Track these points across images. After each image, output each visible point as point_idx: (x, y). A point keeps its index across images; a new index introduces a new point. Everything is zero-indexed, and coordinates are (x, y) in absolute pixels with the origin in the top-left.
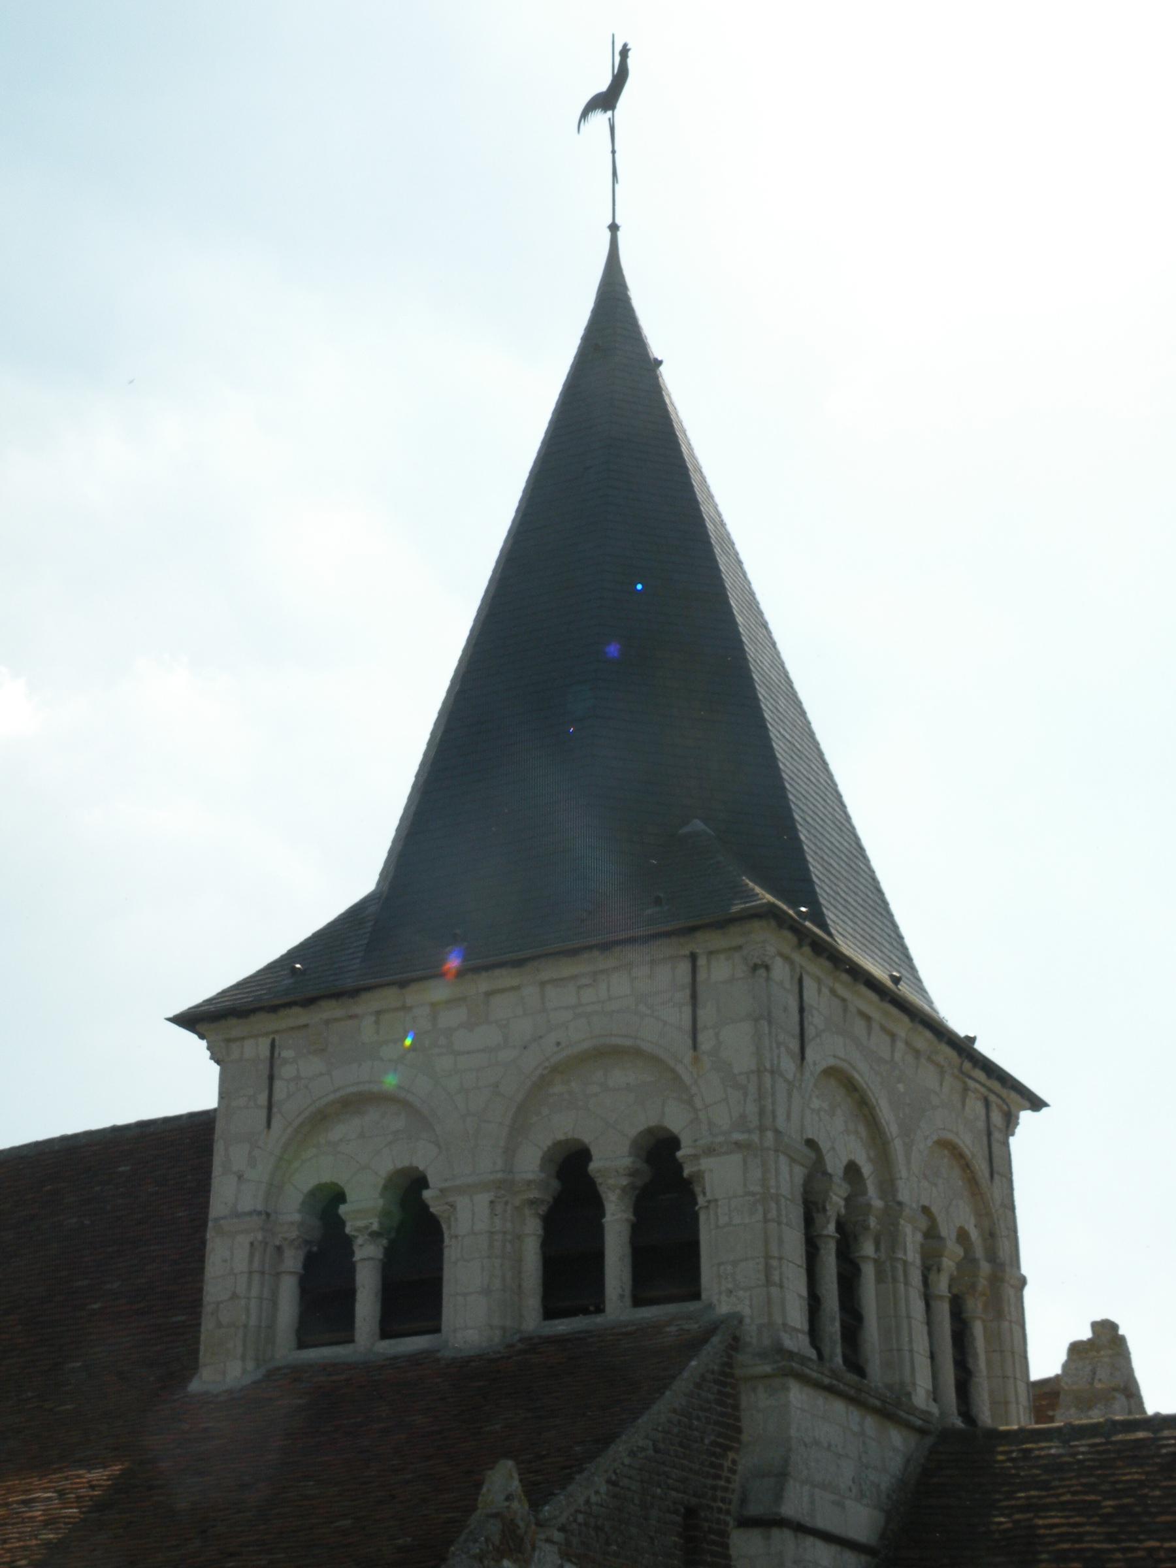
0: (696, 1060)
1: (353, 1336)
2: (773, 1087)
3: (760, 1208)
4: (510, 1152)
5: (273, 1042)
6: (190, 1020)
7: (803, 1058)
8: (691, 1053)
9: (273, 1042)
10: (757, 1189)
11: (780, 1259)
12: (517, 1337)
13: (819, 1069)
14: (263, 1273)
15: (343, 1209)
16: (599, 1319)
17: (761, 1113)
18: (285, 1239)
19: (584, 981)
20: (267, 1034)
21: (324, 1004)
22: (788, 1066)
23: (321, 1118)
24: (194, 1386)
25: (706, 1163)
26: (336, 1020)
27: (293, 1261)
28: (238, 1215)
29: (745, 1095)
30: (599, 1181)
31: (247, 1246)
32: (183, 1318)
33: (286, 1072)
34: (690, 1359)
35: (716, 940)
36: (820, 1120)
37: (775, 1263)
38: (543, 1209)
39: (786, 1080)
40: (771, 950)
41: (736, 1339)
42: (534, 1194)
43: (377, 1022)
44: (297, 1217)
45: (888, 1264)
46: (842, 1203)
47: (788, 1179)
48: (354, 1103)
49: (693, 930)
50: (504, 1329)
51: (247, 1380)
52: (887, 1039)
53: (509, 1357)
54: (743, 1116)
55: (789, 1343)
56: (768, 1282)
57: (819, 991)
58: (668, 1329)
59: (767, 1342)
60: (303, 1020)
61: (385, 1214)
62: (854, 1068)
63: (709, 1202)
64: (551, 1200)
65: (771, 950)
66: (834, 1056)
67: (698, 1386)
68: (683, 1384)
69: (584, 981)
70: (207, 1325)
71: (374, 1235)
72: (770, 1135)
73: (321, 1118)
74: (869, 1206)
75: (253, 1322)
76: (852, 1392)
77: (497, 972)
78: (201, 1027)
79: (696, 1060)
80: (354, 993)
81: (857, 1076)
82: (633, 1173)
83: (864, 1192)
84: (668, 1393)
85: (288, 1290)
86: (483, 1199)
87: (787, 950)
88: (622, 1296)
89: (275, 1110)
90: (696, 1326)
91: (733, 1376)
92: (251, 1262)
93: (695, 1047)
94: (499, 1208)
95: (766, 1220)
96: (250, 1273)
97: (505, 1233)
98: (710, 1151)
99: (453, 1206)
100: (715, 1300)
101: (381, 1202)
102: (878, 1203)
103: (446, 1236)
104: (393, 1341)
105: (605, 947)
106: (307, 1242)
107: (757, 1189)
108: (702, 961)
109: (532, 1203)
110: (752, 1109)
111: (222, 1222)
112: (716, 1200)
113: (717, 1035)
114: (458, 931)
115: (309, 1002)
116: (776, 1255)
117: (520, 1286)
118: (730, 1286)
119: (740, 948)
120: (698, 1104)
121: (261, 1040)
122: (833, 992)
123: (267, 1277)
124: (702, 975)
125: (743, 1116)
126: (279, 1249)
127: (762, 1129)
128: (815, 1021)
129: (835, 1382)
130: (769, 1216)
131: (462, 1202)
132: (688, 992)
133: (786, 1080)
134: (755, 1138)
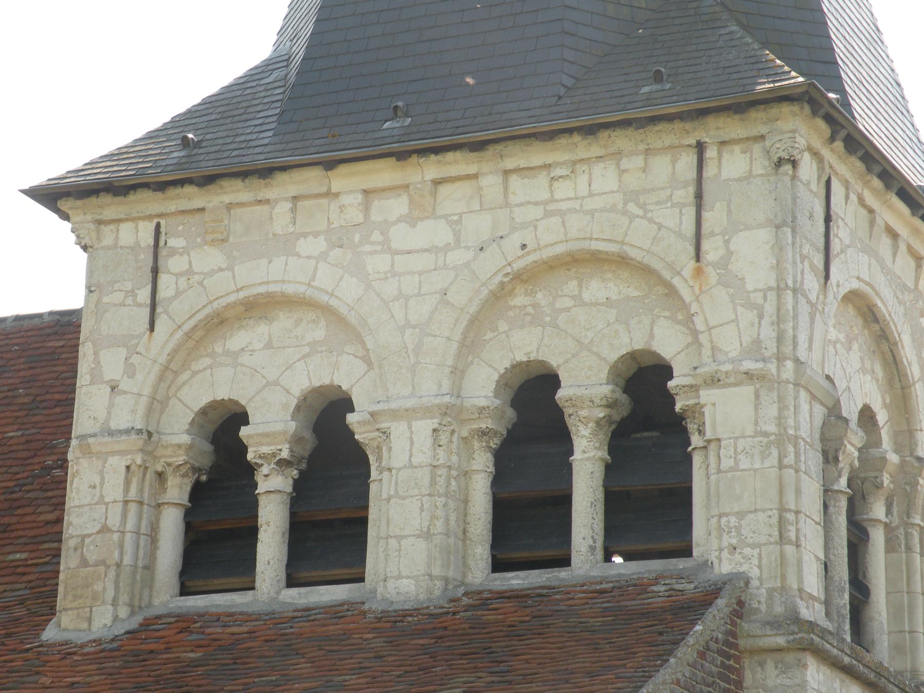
0: (699, 272)
1: (254, 582)
2: (795, 308)
3: (775, 453)
4: (458, 372)
5: (158, 226)
6: (51, 196)
7: (827, 277)
8: (692, 263)
9: (158, 226)
10: (772, 428)
11: (797, 512)
12: (461, 591)
13: (843, 291)
14: (141, 503)
15: (244, 432)
16: (562, 574)
17: (780, 339)
18: (169, 465)
19: (558, 172)
20: (149, 217)
21: (225, 183)
22: (812, 283)
23: (217, 323)
24: (50, 634)
25: (707, 396)
26: (241, 205)
27: (178, 491)
28: (111, 433)
29: (761, 317)
30: (567, 411)
31: (123, 470)
32: (24, 556)
33: (173, 264)
34: (694, 623)
35: (732, 127)
36: (837, 353)
37: (791, 517)
38: (495, 443)
39: (809, 302)
40: (801, 142)
41: (741, 603)
42: (487, 424)
43: (293, 210)
44: (185, 439)
45: (902, 530)
46: (856, 454)
47: (807, 419)
48: (257, 307)
49: (703, 113)
50: (446, 580)
51: (119, 630)
52: (912, 263)
53: (454, 613)
54: (757, 342)
55: (806, 613)
56: (782, 539)
57: (847, 197)
58: (655, 588)
59: (779, 609)
60: (198, 203)
61: (297, 440)
62: (877, 294)
63: (709, 441)
64: (505, 433)
65: (801, 142)
66: (858, 278)
67: (702, 655)
68: (687, 651)
69: (558, 172)
70: (68, 562)
71: (283, 464)
72: (789, 364)
73: (217, 323)
74: (884, 460)
75: (127, 560)
76: (872, 676)
77: (450, 156)
78: (63, 205)
79: (699, 272)
80: (266, 172)
81: (880, 304)
82: (611, 405)
83: (878, 443)
84: (672, 660)
85: (171, 525)
86: (424, 427)
87: (817, 144)
88: (592, 549)
89: (159, 310)
90: (692, 586)
91: (735, 646)
92: (127, 489)
93: (698, 258)
94: (444, 439)
95: (781, 466)
96: (126, 502)
97: (450, 467)
98: (714, 381)
99: (386, 433)
100: (713, 557)
101: (292, 426)
102: (893, 458)
103: (373, 469)
104: (302, 590)
105: (590, 131)
106: (195, 470)
107: (772, 428)
108: (711, 153)
109: (483, 433)
110: (768, 333)
111: (91, 440)
112: (719, 440)
113: (727, 242)
114: (400, 104)
115: (207, 180)
116: (793, 507)
117: (465, 532)
118: (734, 541)
119: (762, 137)
120: (699, 324)
121: (141, 224)
122: (861, 201)
123: (145, 506)
124: (710, 171)
125: (757, 342)
126: (161, 476)
127: (780, 358)
128: (841, 234)
129: (855, 662)
130: (786, 461)
131: (398, 429)
132: (691, 190)
133: (809, 302)
134: (772, 367)
